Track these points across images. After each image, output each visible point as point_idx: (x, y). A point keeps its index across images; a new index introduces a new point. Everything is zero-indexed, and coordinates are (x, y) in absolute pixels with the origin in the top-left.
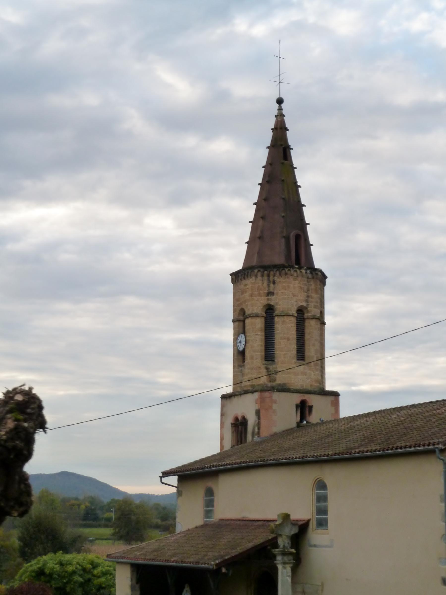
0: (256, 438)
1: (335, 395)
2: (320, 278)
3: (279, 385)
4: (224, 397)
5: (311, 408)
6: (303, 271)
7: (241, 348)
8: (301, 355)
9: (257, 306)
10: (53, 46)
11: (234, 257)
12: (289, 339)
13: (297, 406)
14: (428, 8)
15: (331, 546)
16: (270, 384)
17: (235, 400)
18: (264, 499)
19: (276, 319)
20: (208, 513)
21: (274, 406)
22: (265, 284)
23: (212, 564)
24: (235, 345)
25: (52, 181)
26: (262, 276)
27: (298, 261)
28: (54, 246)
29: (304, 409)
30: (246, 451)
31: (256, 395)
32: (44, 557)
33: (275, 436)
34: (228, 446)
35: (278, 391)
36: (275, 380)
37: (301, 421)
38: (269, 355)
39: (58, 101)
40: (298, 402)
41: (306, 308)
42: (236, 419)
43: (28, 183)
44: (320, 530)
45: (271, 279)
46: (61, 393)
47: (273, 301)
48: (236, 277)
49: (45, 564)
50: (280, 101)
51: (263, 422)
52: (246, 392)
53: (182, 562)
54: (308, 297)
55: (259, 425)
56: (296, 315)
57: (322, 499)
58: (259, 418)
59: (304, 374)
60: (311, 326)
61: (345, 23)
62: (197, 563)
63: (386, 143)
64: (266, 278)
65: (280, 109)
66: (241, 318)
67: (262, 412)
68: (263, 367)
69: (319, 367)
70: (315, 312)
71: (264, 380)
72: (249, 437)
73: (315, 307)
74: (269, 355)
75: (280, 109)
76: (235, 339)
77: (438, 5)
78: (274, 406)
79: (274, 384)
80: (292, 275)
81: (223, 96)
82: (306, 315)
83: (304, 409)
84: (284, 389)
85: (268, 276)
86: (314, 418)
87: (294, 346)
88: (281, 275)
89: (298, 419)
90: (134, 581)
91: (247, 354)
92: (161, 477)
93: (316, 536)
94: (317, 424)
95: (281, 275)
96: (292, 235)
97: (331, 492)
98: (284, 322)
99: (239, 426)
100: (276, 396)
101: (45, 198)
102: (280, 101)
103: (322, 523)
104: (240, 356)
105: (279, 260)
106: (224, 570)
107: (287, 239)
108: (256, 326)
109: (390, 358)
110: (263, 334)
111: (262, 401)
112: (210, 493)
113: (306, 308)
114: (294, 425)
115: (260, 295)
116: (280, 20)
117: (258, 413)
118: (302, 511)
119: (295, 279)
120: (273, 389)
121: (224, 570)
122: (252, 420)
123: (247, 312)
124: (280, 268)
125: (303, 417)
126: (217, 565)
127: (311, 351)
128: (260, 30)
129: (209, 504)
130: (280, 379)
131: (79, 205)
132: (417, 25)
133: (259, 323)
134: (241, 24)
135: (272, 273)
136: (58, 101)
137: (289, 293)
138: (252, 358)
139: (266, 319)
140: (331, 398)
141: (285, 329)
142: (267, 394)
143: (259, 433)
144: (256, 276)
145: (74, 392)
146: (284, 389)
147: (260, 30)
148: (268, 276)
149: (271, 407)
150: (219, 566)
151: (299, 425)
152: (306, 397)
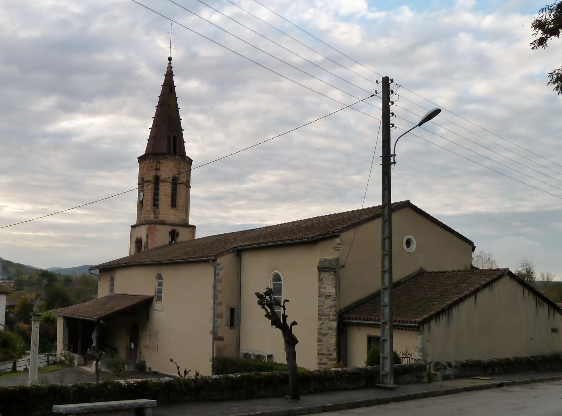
0: (146, 250)
1: (194, 227)
2: (190, 161)
3: (160, 221)
4: (133, 227)
5: (178, 234)
6: (177, 157)
7: (141, 199)
8: (174, 204)
9: (150, 177)
10: (98, 26)
11: (141, 149)
12: (166, 195)
13: (170, 233)
14: (313, 6)
15: (163, 311)
16: (155, 220)
17: (137, 228)
18: (136, 284)
19: (160, 184)
20: (112, 290)
21: (156, 233)
22: (155, 164)
23: (94, 318)
24: (139, 198)
25: (97, 103)
26: (154, 159)
27: (175, 152)
28: (98, 140)
29: (174, 235)
30: (142, 257)
31: (147, 226)
32: (51, 311)
33: (156, 248)
34: (133, 253)
35: (159, 224)
36: (158, 218)
37: (172, 241)
38: (155, 204)
39: (101, 57)
40: (171, 230)
41: (178, 178)
42: (137, 239)
43: (84, 104)
44: (159, 302)
45: (158, 160)
46: (102, 221)
47: (159, 173)
48: (141, 159)
49: (51, 314)
50: (170, 59)
51: (149, 241)
52: (142, 224)
53: (83, 316)
54: (179, 171)
55: (147, 242)
56: (171, 181)
57: (160, 284)
58: (148, 239)
59: (175, 215)
60: (181, 189)
61: (265, 14)
62: (89, 317)
63: (286, 85)
64: (155, 160)
65: (170, 63)
66: (142, 182)
67: (149, 235)
68: (152, 210)
69: (184, 211)
70: (184, 180)
71: (152, 217)
72: (143, 249)
73: (184, 177)
74: (155, 204)
75: (170, 63)
76: (139, 195)
77: (319, 4)
78: (156, 233)
79: (157, 220)
80: (170, 159)
81: (194, 56)
82: (178, 182)
83: (174, 235)
84: (163, 223)
85: (157, 159)
86: (180, 239)
87: (169, 199)
88: (163, 159)
89: (170, 240)
90: (65, 326)
91: (144, 204)
92: (90, 270)
93: (157, 305)
94: (179, 243)
95: (163, 159)
96: (172, 136)
97: (164, 281)
98: (164, 186)
99: (138, 242)
100: (158, 227)
101: (93, 112)
102: (170, 59)
103: (160, 298)
104: (141, 203)
105: (164, 150)
106: (101, 322)
107: (169, 138)
108: (150, 187)
109: (285, 206)
110: (153, 192)
111: (149, 229)
112: (112, 279)
113: (178, 178)
114: (167, 243)
115: (152, 170)
116: (229, 11)
117: (147, 236)
118: (149, 291)
119: (172, 161)
120: (156, 223)
121: (101, 322)
122: (144, 240)
123: (145, 179)
124: (163, 155)
125: (173, 239)
126: (97, 319)
127: (180, 202)
128: (216, 18)
129: (112, 285)
130: (161, 217)
131: (112, 116)
132: (306, 16)
133: (151, 186)
134: (205, 13)
135: (159, 158)
136: (101, 57)
137: (167, 170)
138: (146, 205)
139: (155, 183)
140: (191, 229)
141: (165, 190)
142: (152, 226)
143: (147, 247)
144: (150, 159)
145: (108, 221)
146: (163, 223)
147: (216, 18)
148: (157, 159)
149: (154, 233)
150: (99, 319)
151: (170, 243)
152: (175, 228)
